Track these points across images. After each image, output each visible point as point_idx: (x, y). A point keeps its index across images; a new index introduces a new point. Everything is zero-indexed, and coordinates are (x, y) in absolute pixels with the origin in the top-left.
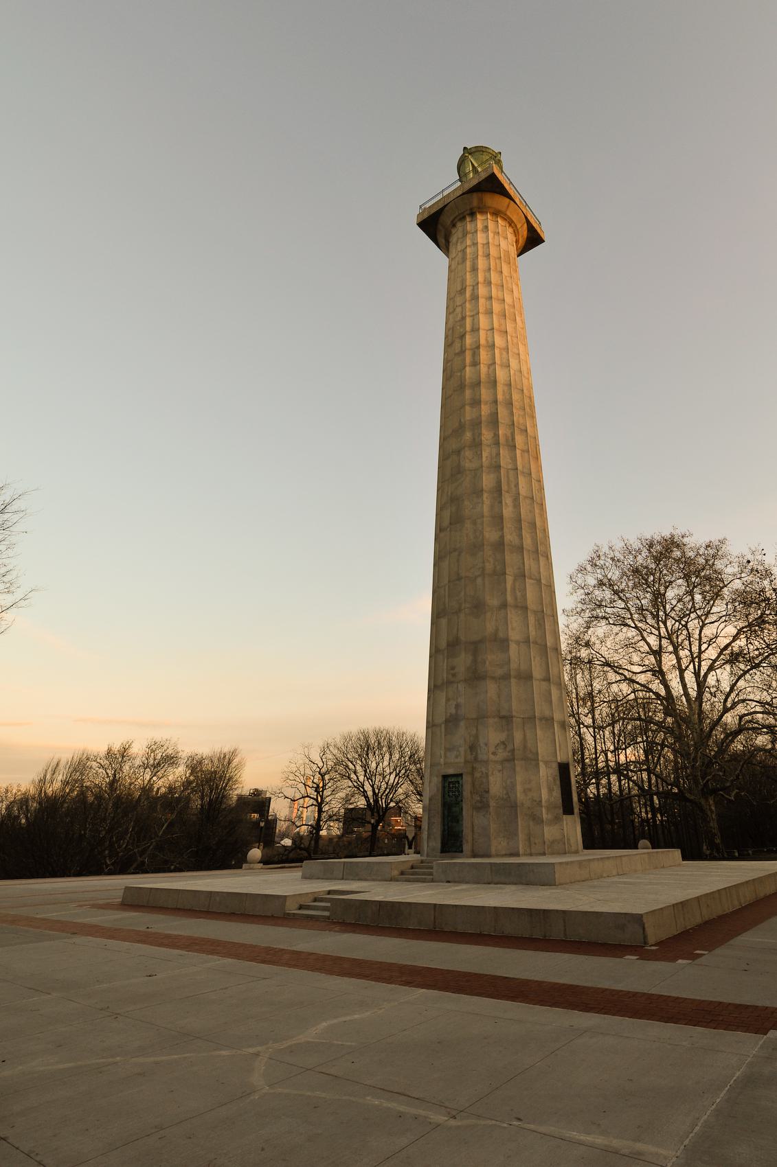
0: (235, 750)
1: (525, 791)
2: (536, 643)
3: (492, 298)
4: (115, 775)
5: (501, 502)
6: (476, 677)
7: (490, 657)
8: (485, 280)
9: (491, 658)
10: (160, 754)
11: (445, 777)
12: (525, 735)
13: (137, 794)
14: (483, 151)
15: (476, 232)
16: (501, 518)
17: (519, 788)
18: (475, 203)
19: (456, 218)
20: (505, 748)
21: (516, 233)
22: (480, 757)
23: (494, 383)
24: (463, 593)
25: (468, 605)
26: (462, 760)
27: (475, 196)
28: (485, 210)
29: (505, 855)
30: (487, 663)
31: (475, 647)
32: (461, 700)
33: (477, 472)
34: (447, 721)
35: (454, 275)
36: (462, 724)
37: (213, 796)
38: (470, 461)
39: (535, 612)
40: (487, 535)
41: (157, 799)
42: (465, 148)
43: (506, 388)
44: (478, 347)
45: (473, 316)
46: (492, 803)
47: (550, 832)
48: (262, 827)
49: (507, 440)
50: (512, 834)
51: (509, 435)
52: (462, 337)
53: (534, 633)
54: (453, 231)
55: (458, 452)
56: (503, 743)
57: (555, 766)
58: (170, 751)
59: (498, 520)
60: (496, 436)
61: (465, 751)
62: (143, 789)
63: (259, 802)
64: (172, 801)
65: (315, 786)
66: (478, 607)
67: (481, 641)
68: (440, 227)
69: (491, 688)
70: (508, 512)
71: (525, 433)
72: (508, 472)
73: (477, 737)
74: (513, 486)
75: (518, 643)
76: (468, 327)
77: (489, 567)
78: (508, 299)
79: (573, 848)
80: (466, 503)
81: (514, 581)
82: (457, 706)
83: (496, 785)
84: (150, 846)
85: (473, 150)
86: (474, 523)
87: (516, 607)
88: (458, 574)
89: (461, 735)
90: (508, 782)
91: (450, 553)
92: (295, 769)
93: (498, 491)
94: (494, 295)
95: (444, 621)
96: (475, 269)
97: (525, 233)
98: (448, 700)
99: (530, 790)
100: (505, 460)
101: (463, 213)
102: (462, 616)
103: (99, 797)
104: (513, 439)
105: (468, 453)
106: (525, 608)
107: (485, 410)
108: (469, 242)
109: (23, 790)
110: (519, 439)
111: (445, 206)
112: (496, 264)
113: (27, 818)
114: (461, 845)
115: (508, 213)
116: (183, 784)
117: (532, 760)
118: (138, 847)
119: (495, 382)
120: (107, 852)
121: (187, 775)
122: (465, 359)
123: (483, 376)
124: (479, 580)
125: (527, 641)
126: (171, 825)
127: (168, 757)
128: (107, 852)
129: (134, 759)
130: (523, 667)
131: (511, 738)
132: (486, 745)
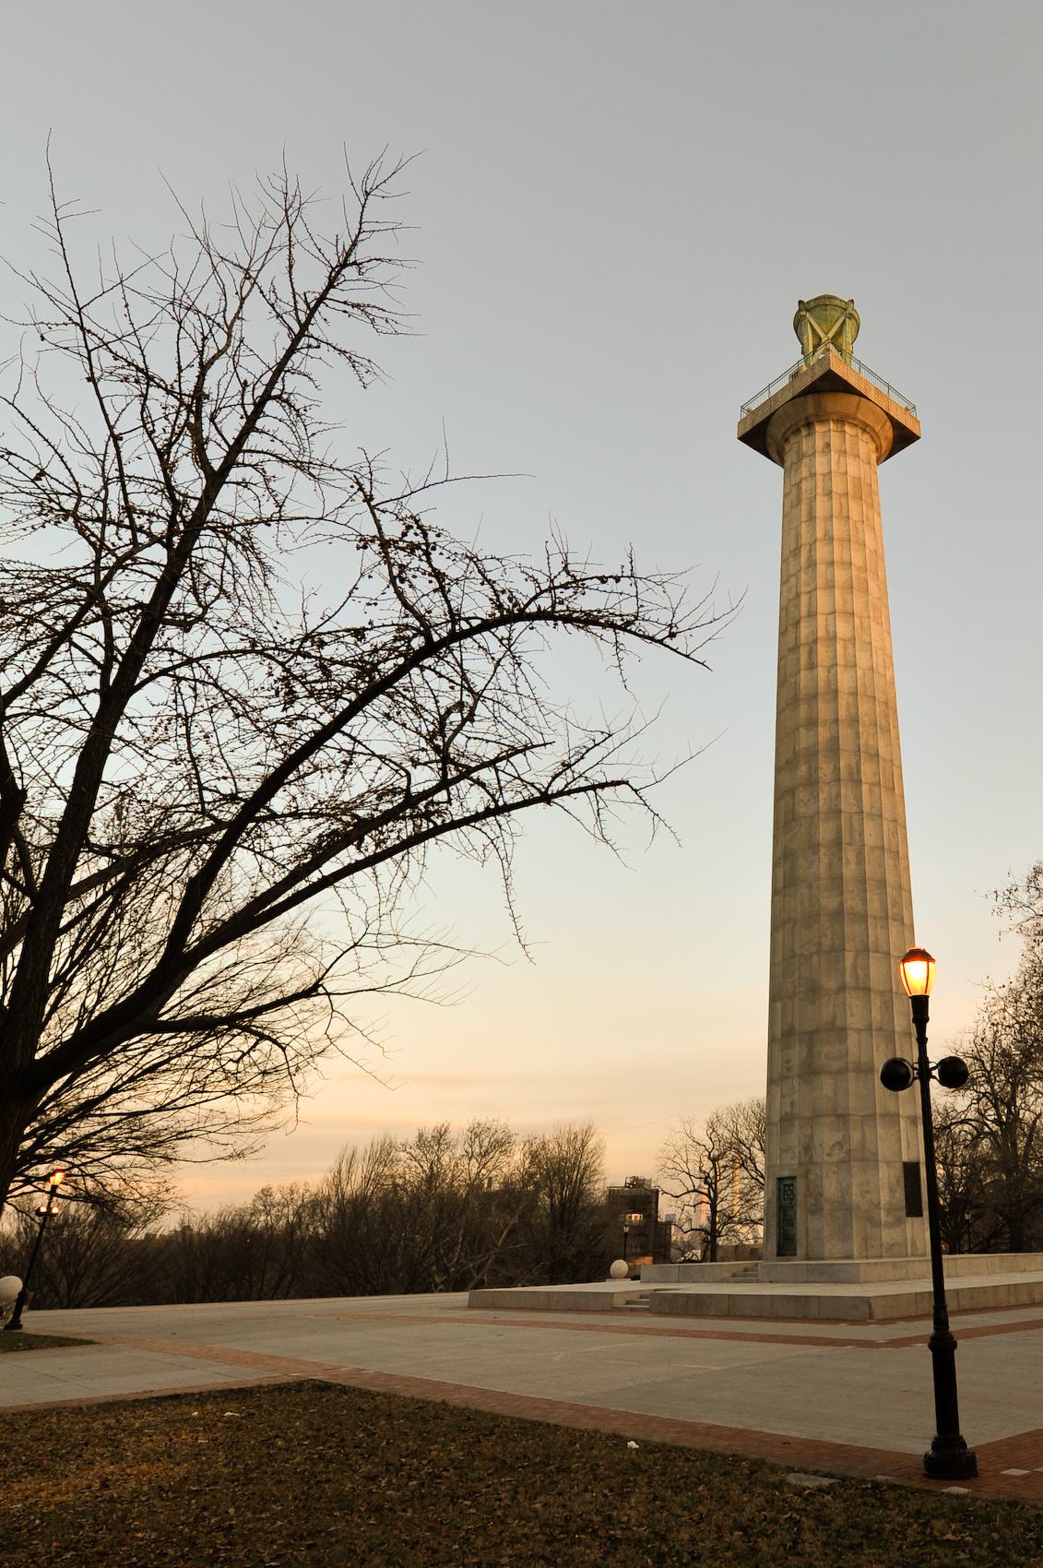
0: (590, 1128)
1: (862, 1195)
2: (880, 1029)
3: (833, 563)
4: (431, 1168)
5: (841, 859)
6: (811, 1072)
7: (826, 1049)
8: (825, 535)
9: (827, 1050)
10: (487, 1140)
11: (780, 1180)
12: (864, 1135)
13: (463, 1192)
14: (826, 305)
15: (814, 454)
16: (841, 878)
17: (855, 1190)
18: (811, 410)
19: (789, 429)
20: (842, 1147)
21: (874, 437)
22: (815, 1158)
23: (834, 694)
24: (797, 975)
25: (802, 989)
26: (797, 1162)
27: (810, 399)
28: (824, 418)
29: (840, 1258)
30: (823, 1055)
31: (810, 1038)
32: (796, 1097)
33: (813, 820)
34: (782, 1120)
35: (794, 499)
36: (797, 1123)
37: (566, 1193)
38: (806, 805)
39: (882, 993)
40: (824, 902)
41: (491, 1196)
42: (800, 302)
43: (851, 698)
44: (815, 641)
45: (810, 592)
46: (827, 1207)
47: (887, 1235)
48: (626, 1234)
49: (851, 773)
50: (846, 1237)
51: (854, 765)
52: (797, 624)
53: (879, 1017)
54: (787, 448)
55: (792, 791)
56: (839, 1143)
57: (900, 1166)
58: (499, 1136)
59: (837, 882)
60: (837, 768)
61: (800, 1153)
62: (471, 1186)
63: (640, 1196)
64: (511, 1196)
65: (703, 1176)
66: (814, 991)
67: (816, 1031)
68: (769, 440)
69: (827, 1084)
70: (849, 871)
71: (875, 759)
72: (851, 817)
73: (812, 1136)
74: (857, 836)
75: (858, 1031)
76: (804, 611)
77: (826, 942)
78: (857, 559)
79: (920, 1251)
80: (801, 861)
81: (856, 957)
82: (792, 1104)
83: (830, 1187)
84: (487, 1261)
85: (812, 304)
86: (810, 887)
87: (857, 988)
88: (793, 951)
89: (795, 1136)
90: (844, 1184)
91: (784, 923)
92: (672, 1155)
93: (837, 844)
94: (836, 558)
95: (779, 1005)
96: (812, 518)
97: (890, 434)
98: (783, 1096)
99: (868, 1192)
100: (847, 805)
101: (796, 424)
102: (796, 1000)
103: (415, 1197)
104: (859, 771)
105: (802, 794)
106: (867, 990)
107: (823, 733)
108: (805, 472)
109: (313, 1190)
110: (867, 770)
111: (772, 414)
112: (841, 505)
113: (325, 1228)
114: (795, 1249)
115: (860, 416)
116: (523, 1180)
117: (870, 1160)
118: (473, 1260)
119: (836, 691)
120: (434, 1268)
121: (527, 1166)
122: (798, 660)
123: (821, 684)
124: (815, 958)
125: (869, 1028)
126: (512, 1232)
127: (498, 1142)
128: (434, 1268)
129: (455, 1146)
130: (864, 1059)
131: (847, 1138)
132: (821, 1145)
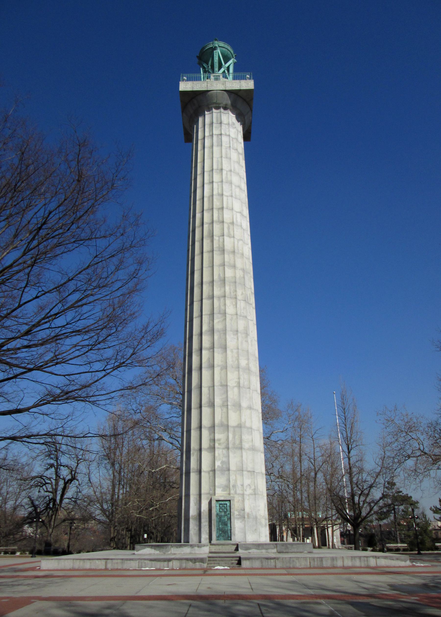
56: (249, 485)
